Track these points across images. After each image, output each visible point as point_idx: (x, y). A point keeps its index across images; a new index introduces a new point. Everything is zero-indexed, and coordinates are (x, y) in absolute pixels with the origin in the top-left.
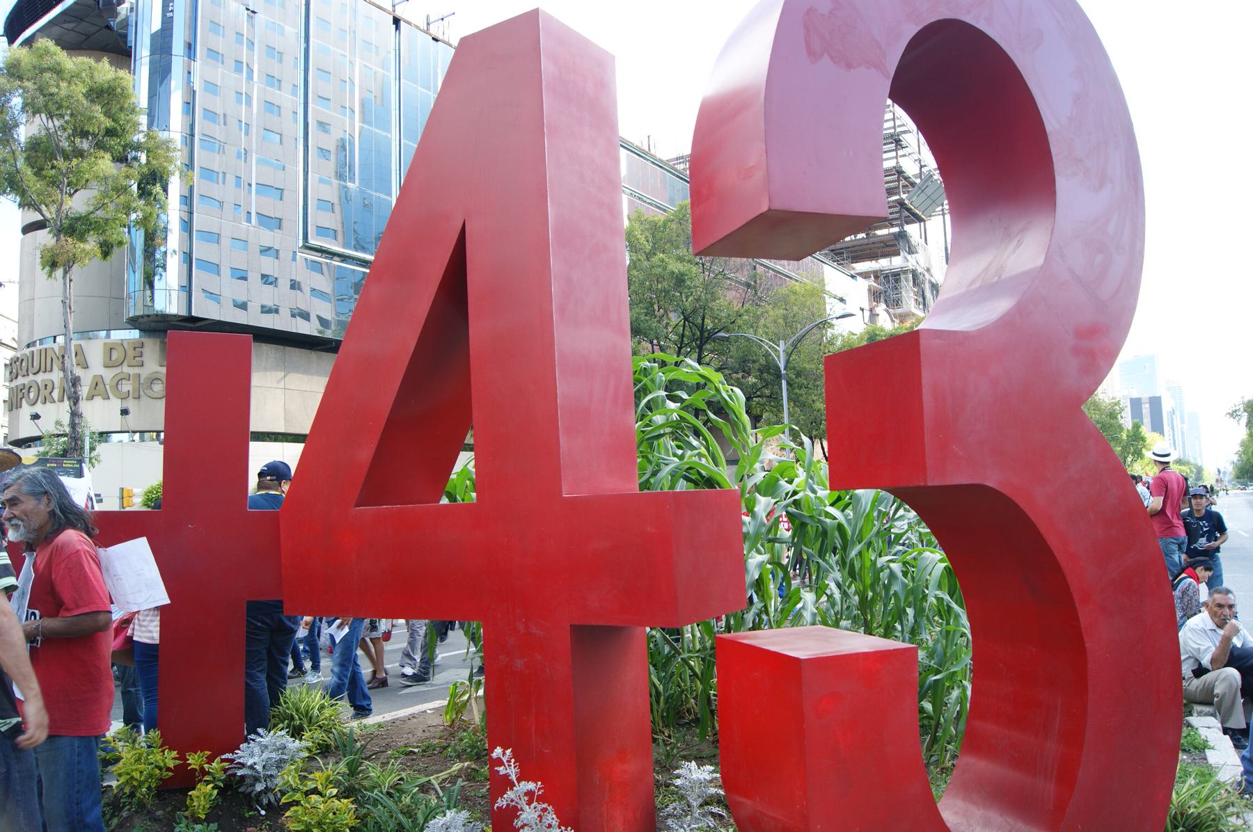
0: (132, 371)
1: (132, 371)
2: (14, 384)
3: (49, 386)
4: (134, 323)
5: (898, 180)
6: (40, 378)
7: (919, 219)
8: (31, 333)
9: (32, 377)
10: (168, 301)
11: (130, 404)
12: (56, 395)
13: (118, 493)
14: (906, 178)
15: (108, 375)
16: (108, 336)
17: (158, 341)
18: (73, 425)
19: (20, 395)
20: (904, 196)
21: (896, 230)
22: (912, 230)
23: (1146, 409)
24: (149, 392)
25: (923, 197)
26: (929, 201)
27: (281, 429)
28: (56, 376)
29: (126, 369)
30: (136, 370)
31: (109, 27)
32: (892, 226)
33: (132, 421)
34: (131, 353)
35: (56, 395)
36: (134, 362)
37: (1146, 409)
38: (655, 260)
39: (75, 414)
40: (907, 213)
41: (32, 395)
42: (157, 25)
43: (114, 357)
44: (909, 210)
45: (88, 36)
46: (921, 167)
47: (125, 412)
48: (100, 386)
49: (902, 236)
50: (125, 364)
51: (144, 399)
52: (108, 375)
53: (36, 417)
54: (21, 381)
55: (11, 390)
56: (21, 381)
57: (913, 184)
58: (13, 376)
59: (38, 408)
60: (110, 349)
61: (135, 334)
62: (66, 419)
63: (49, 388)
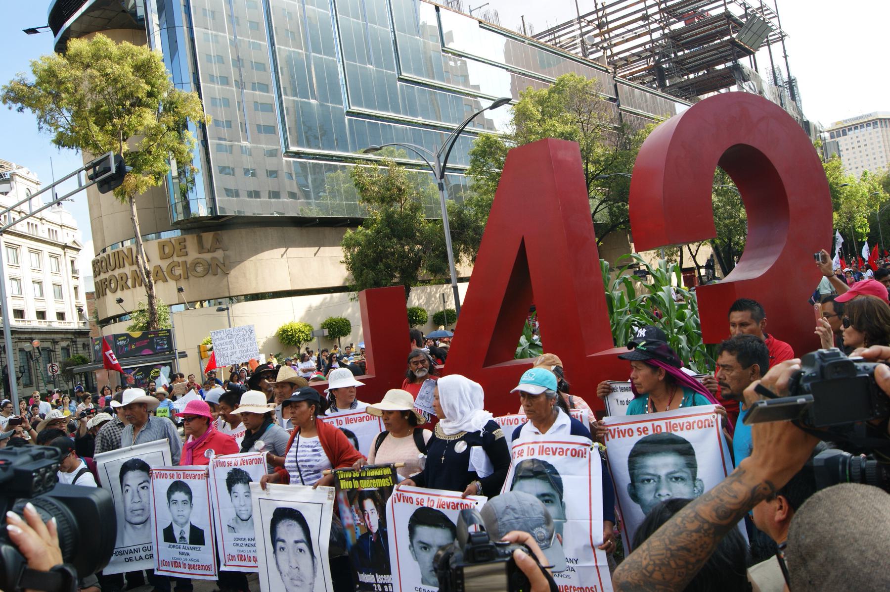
0: (180, 260)
1: (180, 260)
2: (98, 279)
3: (124, 278)
4: (177, 225)
5: (728, 23)
6: (117, 272)
7: (748, 53)
8: (104, 240)
9: (110, 273)
10: (201, 210)
11: (183, 284)
12: (130, 283)
13: (197, 350)
14: (735, 21)
15: (164, 264)
16: (159, 237)
17: (195, 236)
18: (151, 304)
19: (104, 287)
20: (734, 36)
21: (729, 64)
22: (745, 62)
23: (252, 542)
24: (194, 273)
25: (750, 34)
26: (756, 36)
27: (288, 287)
28: (128, 270)
29: (176, 259)
30: (183, 259)
31: (124, 11)
32: (727, 61)
33: (184, 296)
34: (178, 247)
35: (130, 283)
36: (180, 253)
37: (252, 542)
38: (547, 126)
39: (151, 297)
40: (738, 49)
41: (113, 285)
42: (628, 480)
43: (167, 250)
44: (740, 46)
45: (110, 20)
46: (746, 9)
47: (180, 290)
48: (160, 274)
49: (738, 68)
50: (175, 255)
51: (192, 279)
52: (164, 264)
53: (120, 301)
54: (103, 276)
55: (96, 283)
56: (103, 276)
57: (741, 25)
58: (96, 274)
59: (119, 294)
60: (162, 246)
61: (177, 233)
62: (146, 300)
63: (124, 279)
